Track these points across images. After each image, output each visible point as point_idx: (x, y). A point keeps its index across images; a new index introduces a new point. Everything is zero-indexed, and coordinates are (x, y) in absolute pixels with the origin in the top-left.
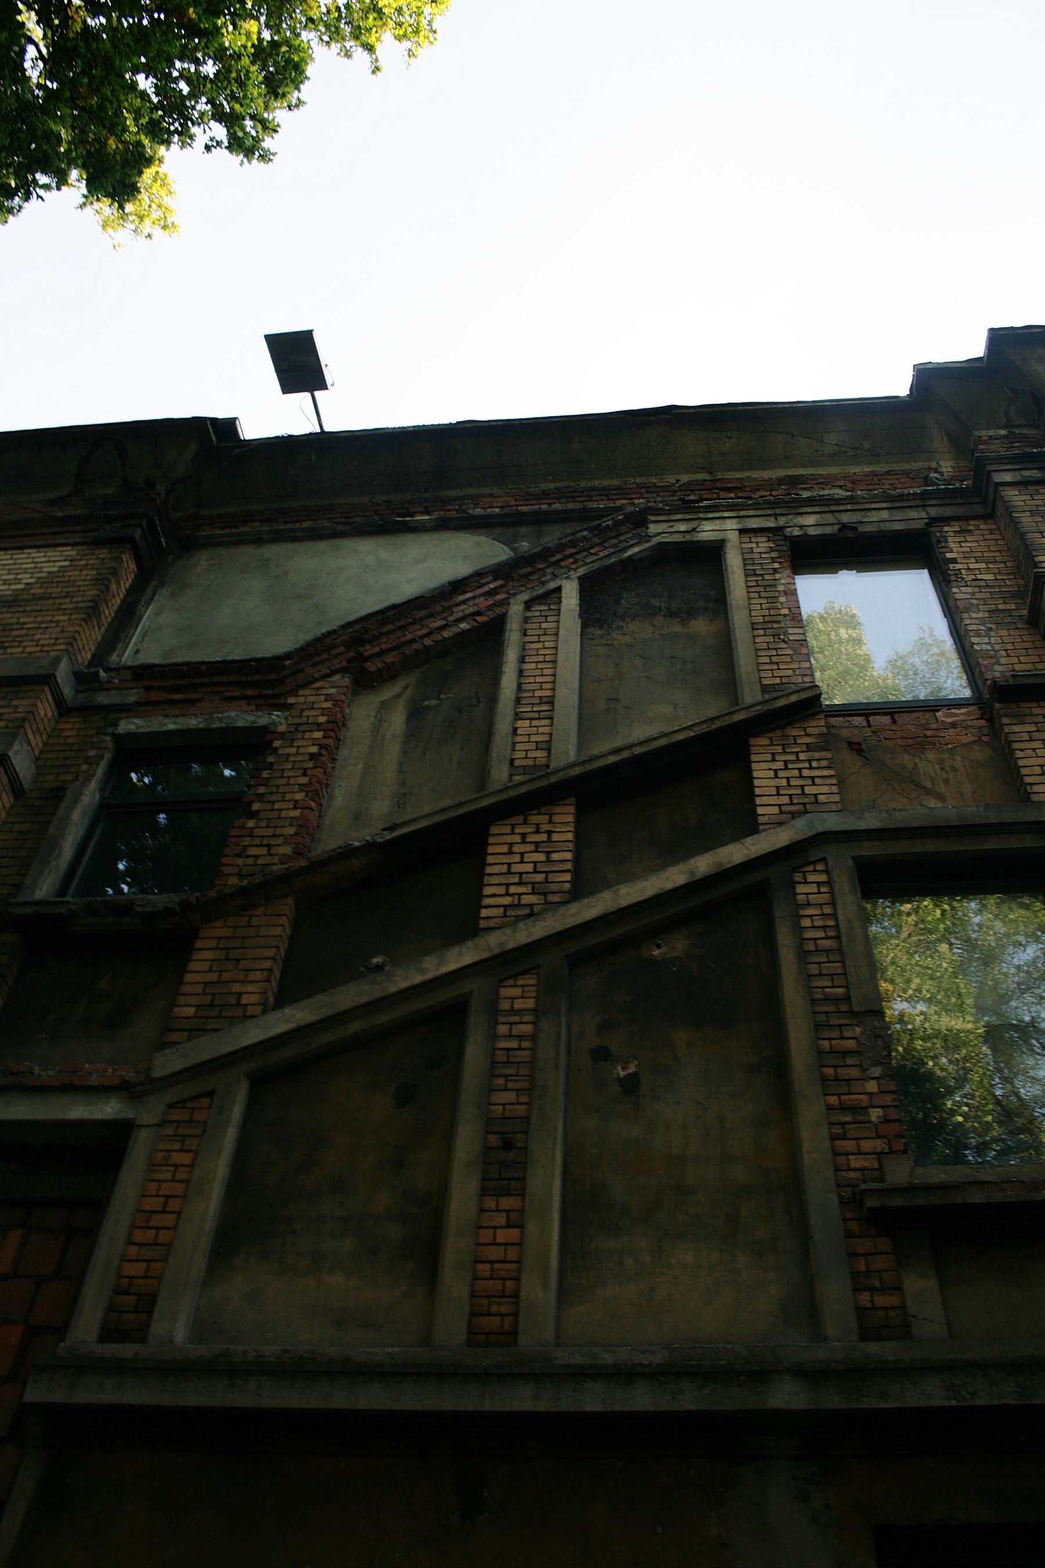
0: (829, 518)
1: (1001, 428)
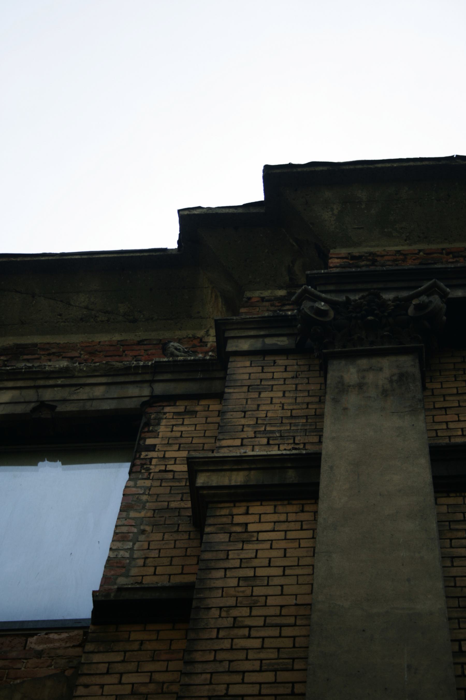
0: (30, 395)
1: (281, 288)
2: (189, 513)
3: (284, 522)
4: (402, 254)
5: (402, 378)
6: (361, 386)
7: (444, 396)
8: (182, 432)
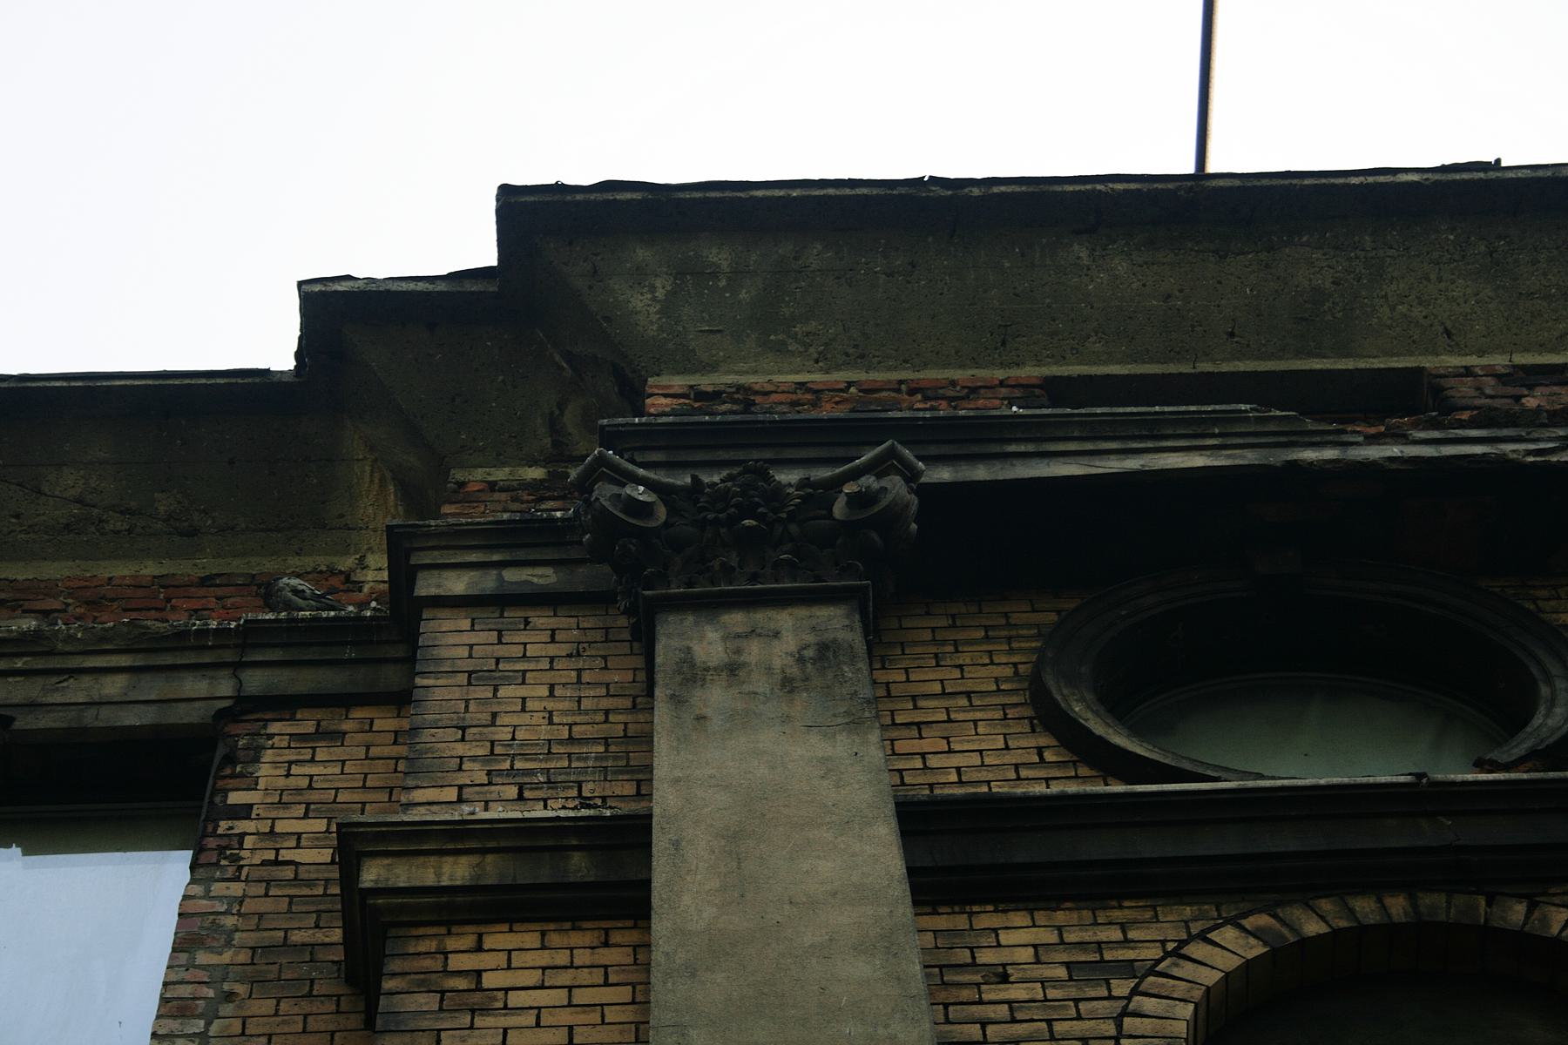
1: (533, 463)
2: (338, 955)
3: (565, 967)
4: (809, 390)
5: (826, 652)
6: (732, 670)
7: (914, 698)
8: (311, 777)
